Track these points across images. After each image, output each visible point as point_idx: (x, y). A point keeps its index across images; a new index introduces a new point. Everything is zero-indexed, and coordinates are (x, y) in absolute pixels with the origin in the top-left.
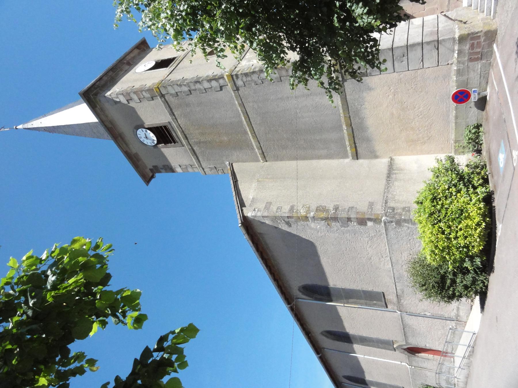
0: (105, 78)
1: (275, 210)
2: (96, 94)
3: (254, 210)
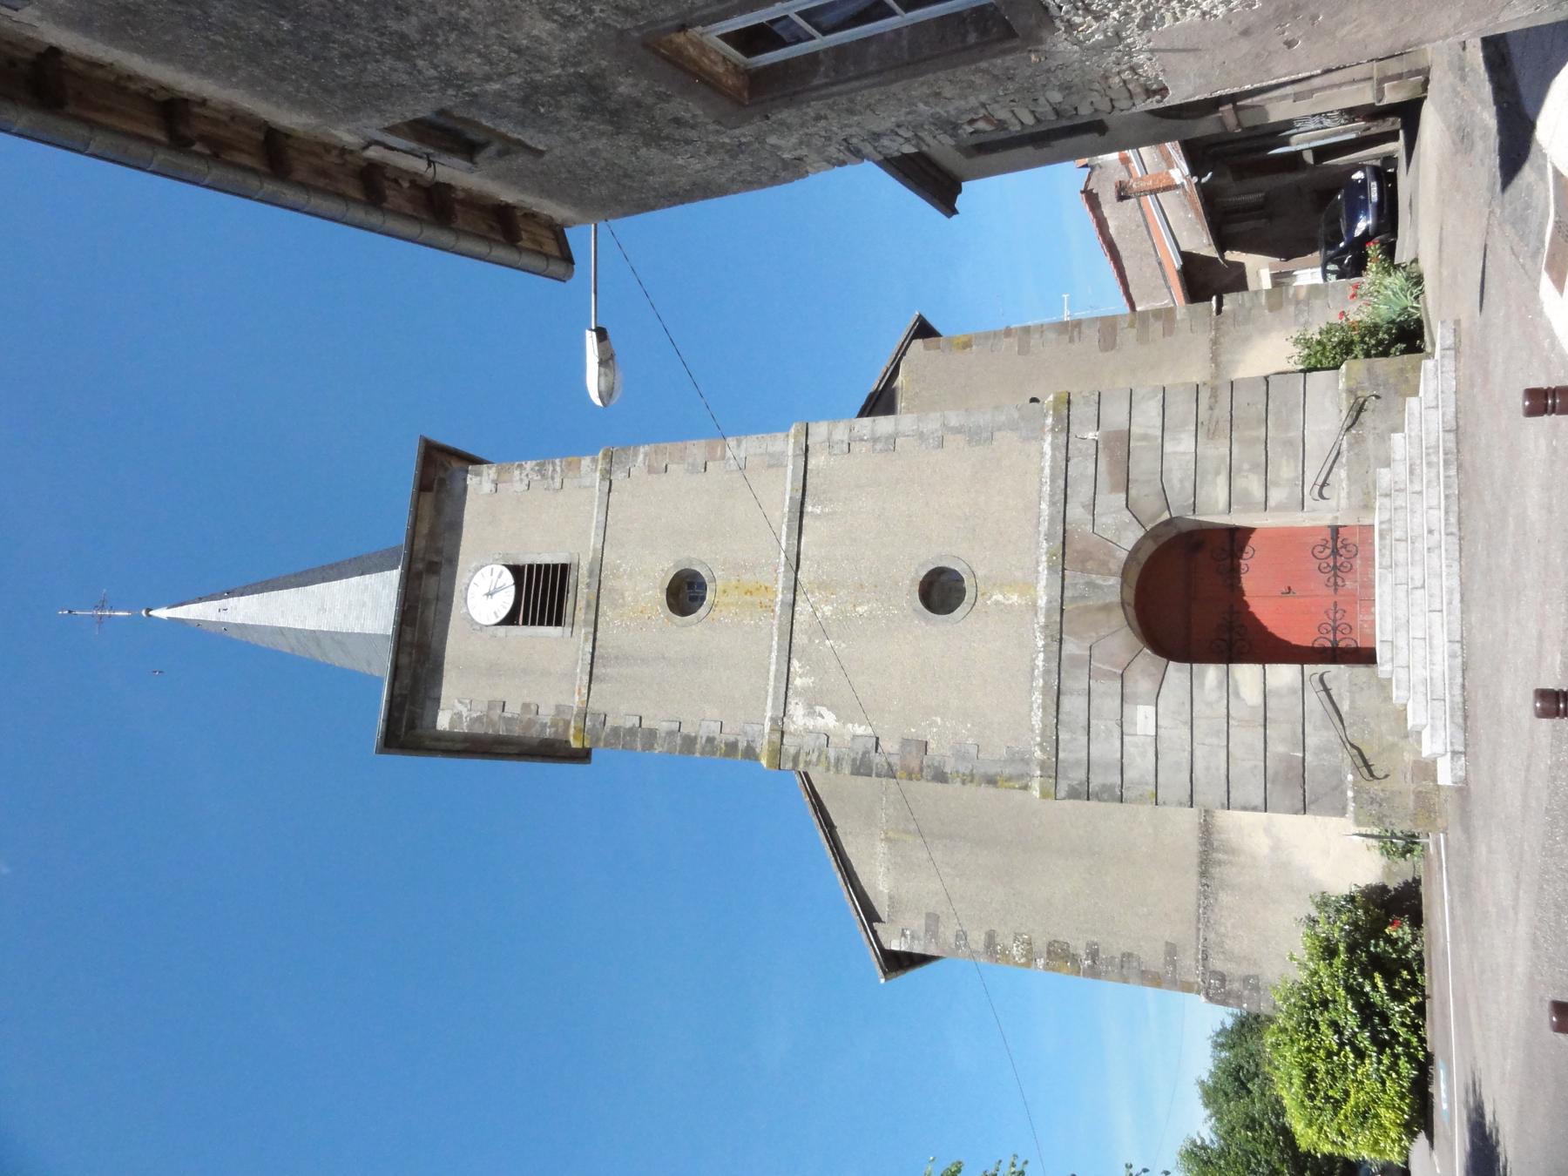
0: (404, 660)
1: (952, 940)
2: (412, 726)
3: (903, 935)
